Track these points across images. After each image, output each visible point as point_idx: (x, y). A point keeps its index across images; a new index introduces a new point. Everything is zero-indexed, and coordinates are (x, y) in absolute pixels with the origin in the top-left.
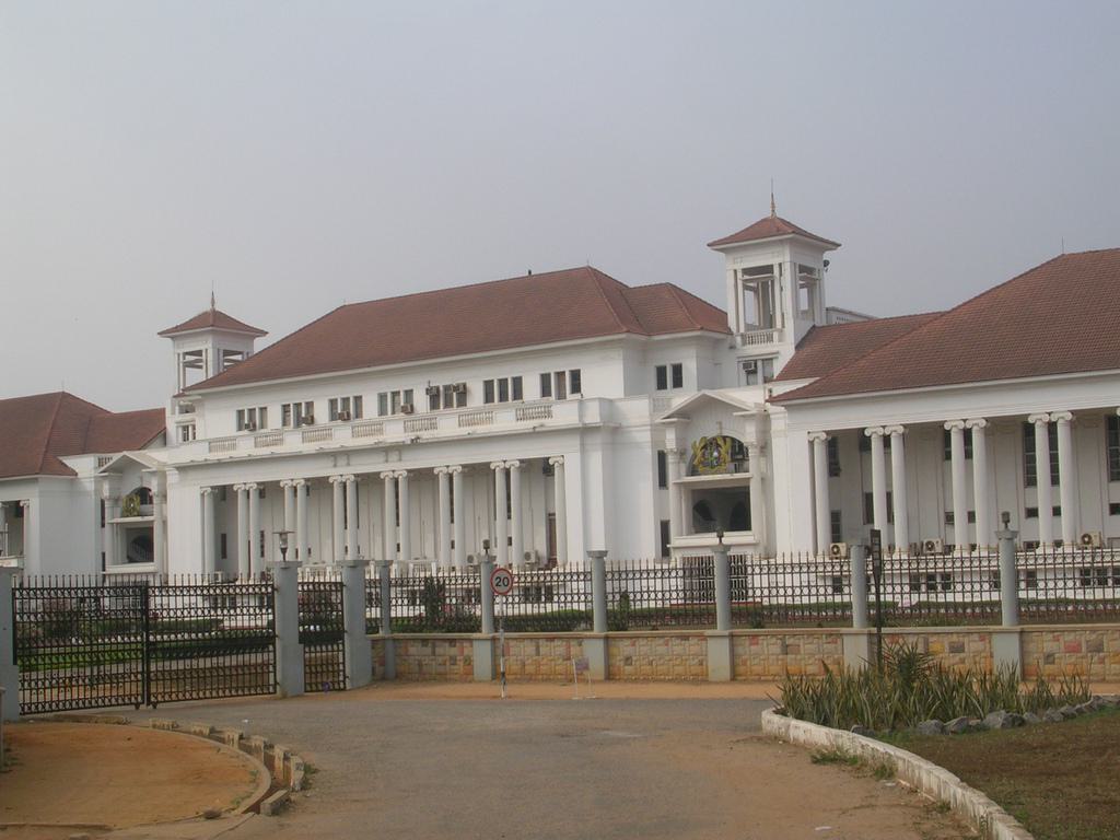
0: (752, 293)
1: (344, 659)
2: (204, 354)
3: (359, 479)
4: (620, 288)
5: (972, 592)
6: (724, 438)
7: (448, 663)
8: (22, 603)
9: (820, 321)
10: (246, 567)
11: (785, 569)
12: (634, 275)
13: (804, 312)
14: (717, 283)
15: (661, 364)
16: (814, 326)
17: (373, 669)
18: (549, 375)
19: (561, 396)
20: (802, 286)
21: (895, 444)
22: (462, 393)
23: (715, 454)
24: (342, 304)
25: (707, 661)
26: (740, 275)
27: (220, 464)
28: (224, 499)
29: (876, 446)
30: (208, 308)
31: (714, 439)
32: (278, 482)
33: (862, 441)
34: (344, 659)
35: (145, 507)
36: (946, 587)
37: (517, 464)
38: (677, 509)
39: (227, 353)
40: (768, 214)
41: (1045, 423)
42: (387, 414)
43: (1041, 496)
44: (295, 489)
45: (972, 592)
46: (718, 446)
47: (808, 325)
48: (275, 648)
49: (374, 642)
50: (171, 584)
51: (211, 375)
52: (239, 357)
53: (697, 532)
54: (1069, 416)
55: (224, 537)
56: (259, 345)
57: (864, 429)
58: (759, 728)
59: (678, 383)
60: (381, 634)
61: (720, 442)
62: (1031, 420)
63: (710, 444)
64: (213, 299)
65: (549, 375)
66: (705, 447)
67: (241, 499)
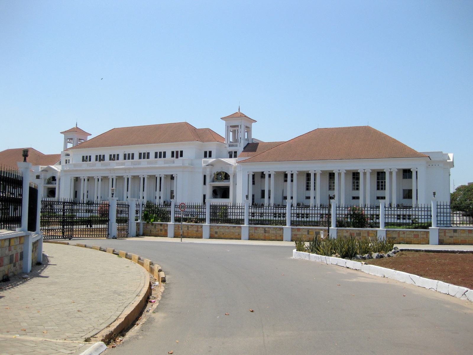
0: (232, 133)
1: (128, 228)
2: (73, 140)
3: (117, 178)
4: (195, 129)
5: (268, 216)
6: (223, 172)
7: (159, 231)
8: (69, 213)
9: (250, 142)
10: (82, 198)
11: (200, 207)
12: (198, 126)
13: (246, 139)
14: (220, 129)
15: (206, 150)
16: (248, 144)
17: (136, 231)
18: (174, 152)
19: (177, 157)
20: (246, 132)
21: (272, 176)
22: (148, 156)
23: (220, 176)
24: (7, 149)
25: (241, 234)
26: (229, 127)
27: (77, 171)
28: (77, 181)
29: (267, 176)
30: (75, 126)
31: (220, 172)
32: (94, 177)
33: (263, 175)
34: (128, 228)
35: (54, 182)
36: (307, 217)
37: (147, 176)
38: (209, 192)
39: (80, 139)
40: (238, 111)
41: (363, 172)
42: (157, 158)
43: (311, 193)
44: (98, 179)
45: (268, 216)
46: (221, 174)
47: (246, 143)
48: (108, 223)
49: (137, 223)
50: (60, 201)
51: (75, 145)
52: (83, 141)
53: (213, 198)
54: (320, 172)
55: (76, 192)
56: (89, 138)
57: (264, 172)
58: (93, 224)
59: (210, 156)
60: (139, 221)
61: (222, 173)
62: (287, 173)
63: (219, 174)
64: (77, 124)
65: (174, 152)
66: (218, 174)
67: (82, 180)
